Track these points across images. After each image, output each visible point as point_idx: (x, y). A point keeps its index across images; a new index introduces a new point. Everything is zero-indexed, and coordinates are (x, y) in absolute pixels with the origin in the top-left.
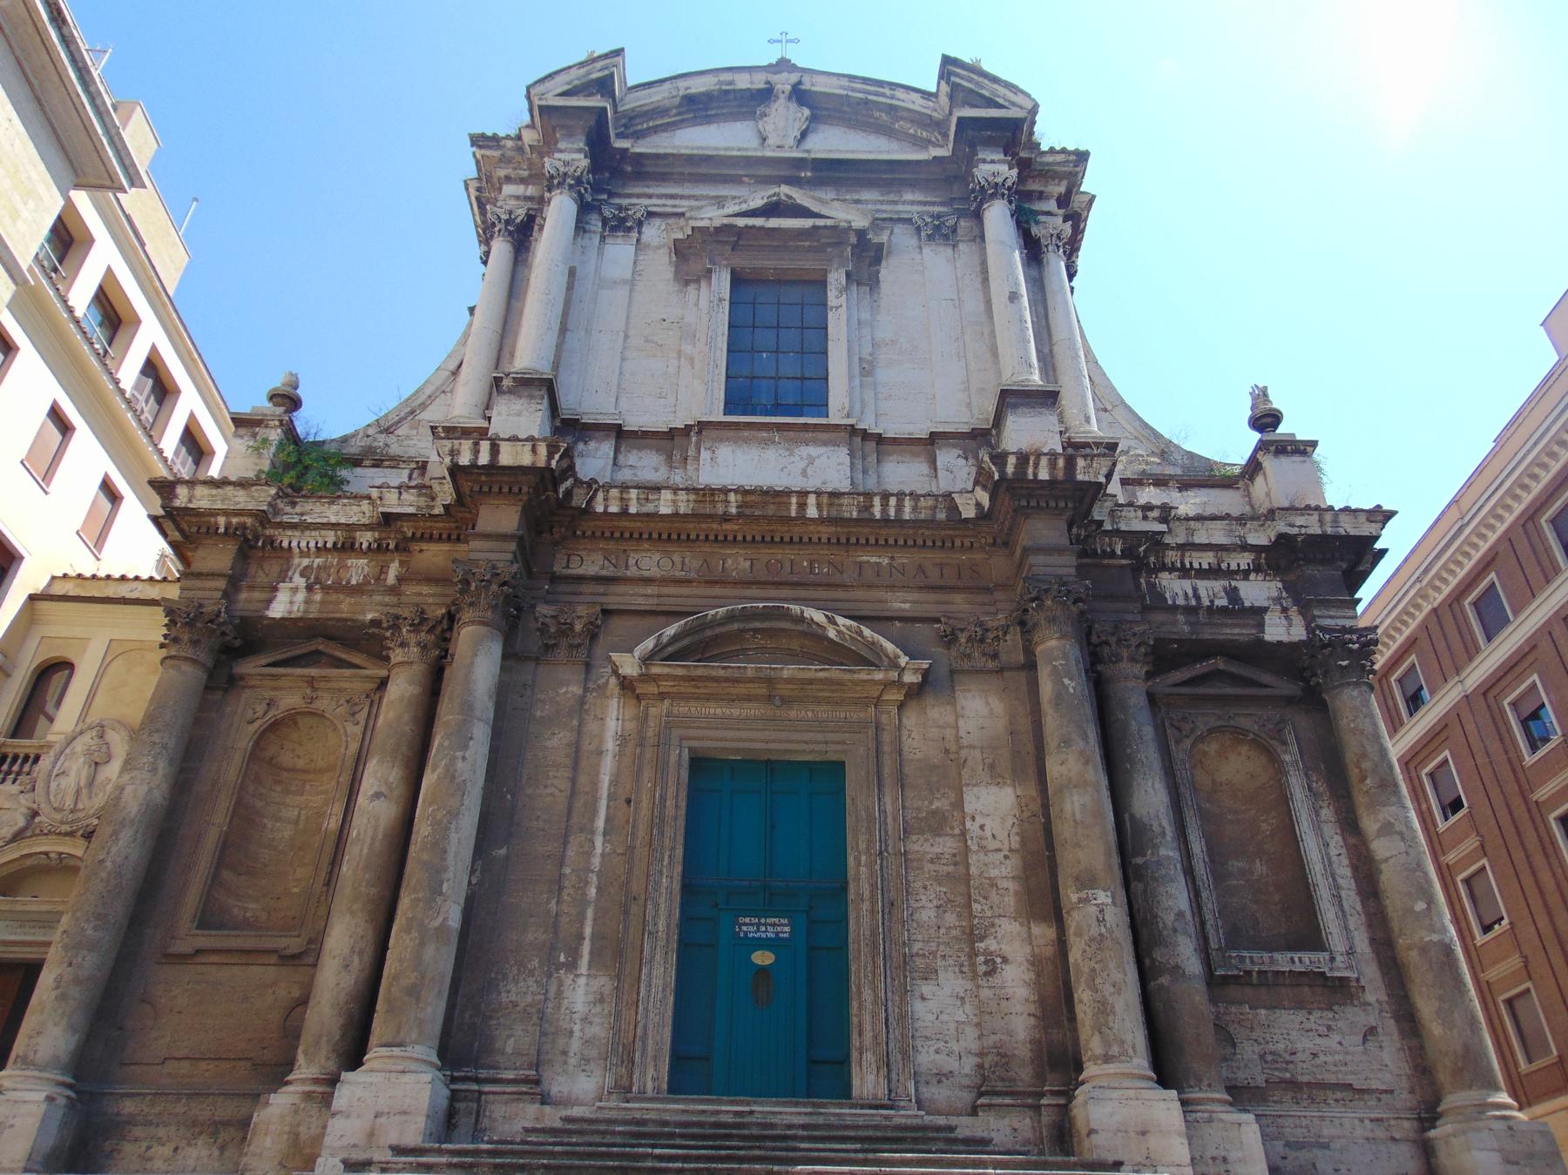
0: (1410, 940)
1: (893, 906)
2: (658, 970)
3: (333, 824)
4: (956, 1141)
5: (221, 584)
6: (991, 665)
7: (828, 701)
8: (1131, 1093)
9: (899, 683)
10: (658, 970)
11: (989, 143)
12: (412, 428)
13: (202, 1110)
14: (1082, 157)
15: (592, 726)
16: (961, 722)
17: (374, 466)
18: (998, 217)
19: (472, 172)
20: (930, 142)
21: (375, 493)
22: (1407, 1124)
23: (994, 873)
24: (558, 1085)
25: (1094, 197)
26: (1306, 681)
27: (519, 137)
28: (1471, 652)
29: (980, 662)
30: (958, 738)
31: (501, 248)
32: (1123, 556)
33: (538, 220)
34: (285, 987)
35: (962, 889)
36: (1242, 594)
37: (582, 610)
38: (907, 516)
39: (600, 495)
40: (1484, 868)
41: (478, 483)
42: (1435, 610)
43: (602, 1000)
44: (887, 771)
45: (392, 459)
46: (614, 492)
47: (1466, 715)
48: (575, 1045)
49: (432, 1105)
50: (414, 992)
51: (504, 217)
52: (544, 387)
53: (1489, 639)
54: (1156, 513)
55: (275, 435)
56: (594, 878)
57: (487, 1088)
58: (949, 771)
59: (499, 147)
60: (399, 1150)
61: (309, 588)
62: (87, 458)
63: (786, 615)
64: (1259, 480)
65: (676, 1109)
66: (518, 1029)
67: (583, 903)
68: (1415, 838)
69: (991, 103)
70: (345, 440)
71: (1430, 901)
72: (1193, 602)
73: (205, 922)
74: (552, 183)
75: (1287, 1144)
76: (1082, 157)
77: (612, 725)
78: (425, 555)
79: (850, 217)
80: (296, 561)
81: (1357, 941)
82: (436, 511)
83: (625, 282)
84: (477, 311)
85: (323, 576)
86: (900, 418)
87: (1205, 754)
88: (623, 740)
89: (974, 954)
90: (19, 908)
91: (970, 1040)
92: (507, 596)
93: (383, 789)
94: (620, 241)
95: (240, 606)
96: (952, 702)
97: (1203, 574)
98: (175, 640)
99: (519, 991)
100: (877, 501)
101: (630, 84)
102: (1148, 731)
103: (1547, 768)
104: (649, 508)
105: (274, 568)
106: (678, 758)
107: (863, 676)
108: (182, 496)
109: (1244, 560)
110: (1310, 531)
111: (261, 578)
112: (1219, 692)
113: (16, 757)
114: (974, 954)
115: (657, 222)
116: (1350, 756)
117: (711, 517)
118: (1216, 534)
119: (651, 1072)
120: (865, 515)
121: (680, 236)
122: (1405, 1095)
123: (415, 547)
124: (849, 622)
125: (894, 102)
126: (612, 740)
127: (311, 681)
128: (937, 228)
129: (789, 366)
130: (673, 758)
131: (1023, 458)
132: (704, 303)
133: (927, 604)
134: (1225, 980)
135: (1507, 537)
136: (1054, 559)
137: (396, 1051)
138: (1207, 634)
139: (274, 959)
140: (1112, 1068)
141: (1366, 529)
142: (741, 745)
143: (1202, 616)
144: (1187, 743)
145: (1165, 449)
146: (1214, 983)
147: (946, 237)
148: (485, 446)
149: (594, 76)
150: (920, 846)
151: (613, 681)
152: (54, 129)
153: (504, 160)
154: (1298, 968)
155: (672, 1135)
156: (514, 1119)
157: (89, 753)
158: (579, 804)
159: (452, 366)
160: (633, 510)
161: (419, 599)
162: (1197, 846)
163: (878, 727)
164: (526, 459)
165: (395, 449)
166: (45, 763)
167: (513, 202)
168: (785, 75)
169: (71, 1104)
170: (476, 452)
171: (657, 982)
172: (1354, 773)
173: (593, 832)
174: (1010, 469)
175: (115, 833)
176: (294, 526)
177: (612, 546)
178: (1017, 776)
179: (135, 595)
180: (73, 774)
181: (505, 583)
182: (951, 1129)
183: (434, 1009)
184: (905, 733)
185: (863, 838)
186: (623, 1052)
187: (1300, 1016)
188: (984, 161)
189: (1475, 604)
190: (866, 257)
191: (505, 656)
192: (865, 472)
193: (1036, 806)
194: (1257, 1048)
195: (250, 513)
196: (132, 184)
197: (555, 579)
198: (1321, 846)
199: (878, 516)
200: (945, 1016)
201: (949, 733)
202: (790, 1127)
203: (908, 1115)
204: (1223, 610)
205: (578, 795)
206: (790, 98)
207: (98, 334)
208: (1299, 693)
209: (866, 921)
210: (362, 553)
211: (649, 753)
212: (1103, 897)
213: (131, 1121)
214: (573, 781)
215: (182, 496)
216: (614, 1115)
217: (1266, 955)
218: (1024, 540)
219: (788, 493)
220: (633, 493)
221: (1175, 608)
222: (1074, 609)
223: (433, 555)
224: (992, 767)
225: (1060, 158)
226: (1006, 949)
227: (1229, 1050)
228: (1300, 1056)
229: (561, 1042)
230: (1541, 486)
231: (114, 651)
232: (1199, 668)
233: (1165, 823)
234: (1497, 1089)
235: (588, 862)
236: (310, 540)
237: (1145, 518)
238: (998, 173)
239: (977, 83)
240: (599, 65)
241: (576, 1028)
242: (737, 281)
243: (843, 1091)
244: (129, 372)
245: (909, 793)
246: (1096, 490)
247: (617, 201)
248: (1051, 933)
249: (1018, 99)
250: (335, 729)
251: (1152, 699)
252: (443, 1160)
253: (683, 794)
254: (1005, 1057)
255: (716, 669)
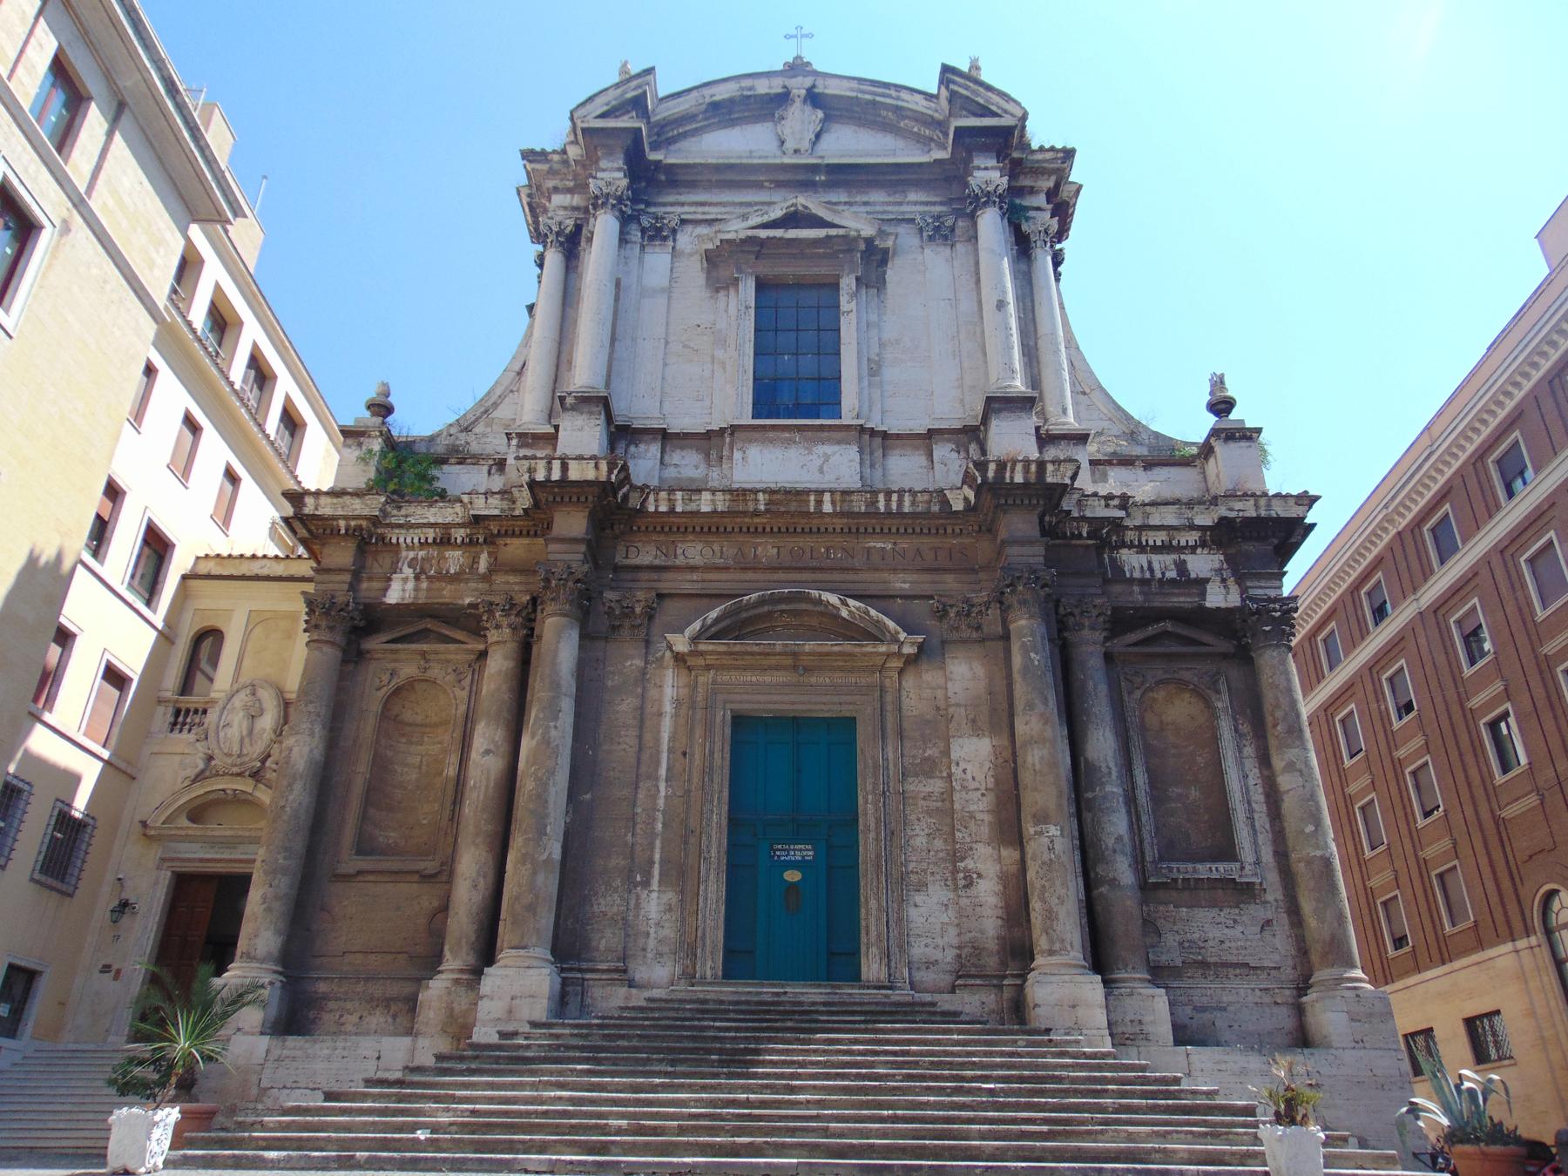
0: (1300, 854)
1: (893, 834)
2: (712, 887)
3: (451, 771)
4: (934, 1013)
5: (347, 577)
6: (974, 635)
7: (841, 669)
8: (1067, 978)
9: (899, 654)
10: (712, 887)
11: (985, 149)
12: (487, 426)
13: (377, 990)
14: (1069, 154)
15: (653, 693)
16: (950, 685)
17: (459, 463)
18: (990, 223)
19: (523, 180)
20: (932, 139)
21: (466, 498)
22: (1287, 992)
23: (972, 808)
24: (640, 972)
25: (1080, 187)
26: (1239, 639)
27: (564, 152)
28: (1427, 573)
29: (966, 633)
30: (947, 698)
31: (554, 258)
32: (1089, 537)
33: (584, 231)
34: (428, 899)
35: (948, 820)
36: (1190, 566)
37: (640, 595)
38: (906, 510)
39: (652, 498)
40: (1426, 764)
41: (550, 496)
42: (1399, 533)
43: (670, 910)
44: (889, 726)
45: (474, 456)
46: (663, 495)
47: (1419, 630)
48: (652, 943)
49: (551, 990)
50: (531, 909)
51: (555, 229)
52: (601, 403)
53: (1331, 669)
54: (1116, 502)
55: (376, 445)
56: (660, 816)
57: (588, 976)
58: (939, 725)
59: (547, 161)
60: (534, 1024)
61: (417, 578)
62: (214, 451)
63: (807, 598)
64: (1212, 460)
65: (729, 991)
66: (608, 933)
67: (652, 835)
68: (1311, 774)
69: (986, 112)
70: (432, 439)
71: (1318, 823)
72: (1148, 575)
73: (364, 847)
74: (597, 202)
75: (1195, 1008)
76: (1069, 154)
77: (669, 692)
78: (509, 548)
79: (858, 226)
80: (404, 554)
81: (1263, 853)
82: (517, 513)
83: (663, 290)
84: (538, 311)
85: (427, 566)
86: (905, 417)
87: (1154, 700)
88: (678, 703)
89: (955, 871)
90: (209, 833)
91: (951, 937)
92: (580, 591)
93: (492, 747)
94: (657, 249)
95: (362, 594)
96: (943, 668)
97: (1156, 549)
98: (316, 627)
99: (607, 903)
100: (881, 497)
101: (661, 95)
102: (1103, 688)
103: (1481, 680)
104: (692, 507)
105: (386, 560)
106: (723, 717)
107: (869, 649)
108: (310, 506)
109: (1192, 537)
110: (1247, 514)
111: (377, 569)
112: (1167, 650)
113: (188, 711)
114: (955, 871)
115: (689, 228)
116: (1267, 708)
117: (745, 513)
118: (1169, 517)
119: (709, 963)
120: (872, 510)
121: (710, 246)
122: (1290, 970)
123: (501, 541)
124: (858, 604)
125: (900, 103)
126: (670, 702)
127: (423, 654)
128: (937, 229)
129: (808, 364)
130: (719, 719)
131: (1001, 466)
132: (732, 310)
133: (924, 582)
134: (1157, 886)
135: (1460, 473)
136: (1028, 550)
137: (522, 952)
138: (1158, 603)
139: (416, 877)
140: (1054, 959)
141: (1293, 512)
142: (772, 707)
143: (1154, 587)
144: (1138, 694)
145: (1134, 430)
146: (1146, 889)
147: (946, 238)
148: (556, 465)
149: (630, 95)
150: (915, 786)
151: (668, 654)
152: (175, 184)
153: (552, 172)
154: (1215, 875)
155: (728, 1011)
156: (611, 999)
157: (246, 708)
158: (645, 757)
159: (517, 367)
160: (679, 509)
161: (507, 587)
162: (1141, 778)
163: (882, 689)
164: (591, 475)
165: (475, 448)
166: (212, 717)
167: (561, 213)
168: (800, 79)
169: (284, 986)
170: (549, 469)
171: (712, 896)
172: (1269, 720)
173: (657, 779)
174: (991, 474)
175: (290, 785)
176: (400, 526)
177: (662, 538)
178: (994, 729)
179: (265, 572)
180: (236, 724)
181: (578, 581)
182: (933, 1004)
183: (546, 920)
184: (904, 693)
185: (870, 781)
186: (688, 948)
187: (1214, 912)
188: (979, 168)
189: (1433, 530)
190: (874, 260)
191: (582, 637)
192: (872, 466)
193: (1007, 754)
194: (1178, 938)
195: (365, 518)
196: (236, 215)
197: (617, 569)
198: (1240, 779)
199: (882, 510)
200: (932, 919)
201: (940, 694)
202: (814, 1004)
203: (902, 995)
204: (1173, 581)
205: (644, 751)
206: (805, 101)
207: (211, 340)
208: (1232, 650)
209: (872, 846)
210: (455, 546)
211: (699, 714)
212: (1054, 831)
213: (325, 997)
214: (640, 737)
215: (310, 506)
216: (680, 996)
217: (1190, 866)
218: (1003, 534)
219: (807, 492)
220: (679, 495)
221: (1132, 580)
222: (1042, 593)
223: (516, 548)
224: (974, 721)
225: (1049, 155)
226: (981, 867)
227: (1156, 939)
228: (1210, 943)
229: (641, 941)
230: (1489, 430)
231: (256, 620)
232: (1151, 630)
233: (1112, 765)
234: (1353, 966)
235: (655, 803)
236: (414, 536)
237: (1107, 506)
238: (994, 174)
239: (973, 92)
240: (634, 83)
241: (652, 931)
242: (762, 286)
243: (855, 976)
244: (238, 370)
245: (908, 744)
246: (1063, 489)
247: (652, 210)
248: (1016, 855)
249: (1010, 107)
250: (445, 692)
251: (1108, 657)
252: (567, 1031)
253: (727, 748)
254: (977, 950)
255: (751, 645)
